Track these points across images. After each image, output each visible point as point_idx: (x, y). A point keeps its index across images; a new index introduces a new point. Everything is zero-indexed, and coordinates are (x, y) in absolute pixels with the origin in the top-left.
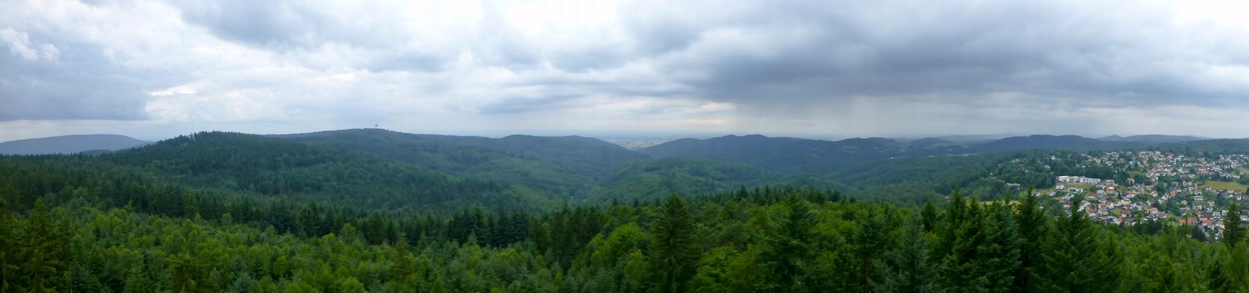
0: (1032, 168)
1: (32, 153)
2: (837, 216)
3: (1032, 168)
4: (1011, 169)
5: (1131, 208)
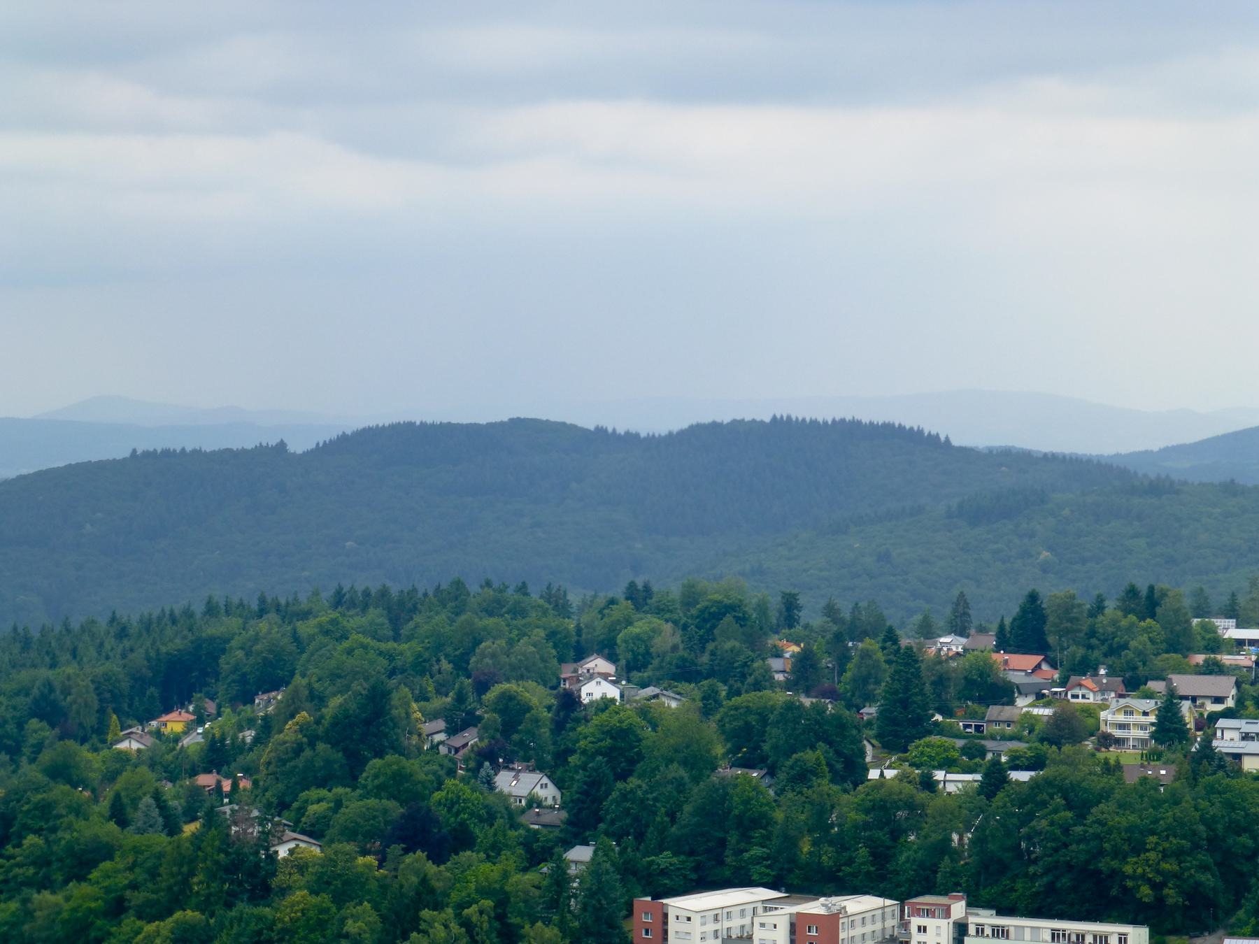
0: (356, 805)
3: (356, 805)
4: (100, 828)
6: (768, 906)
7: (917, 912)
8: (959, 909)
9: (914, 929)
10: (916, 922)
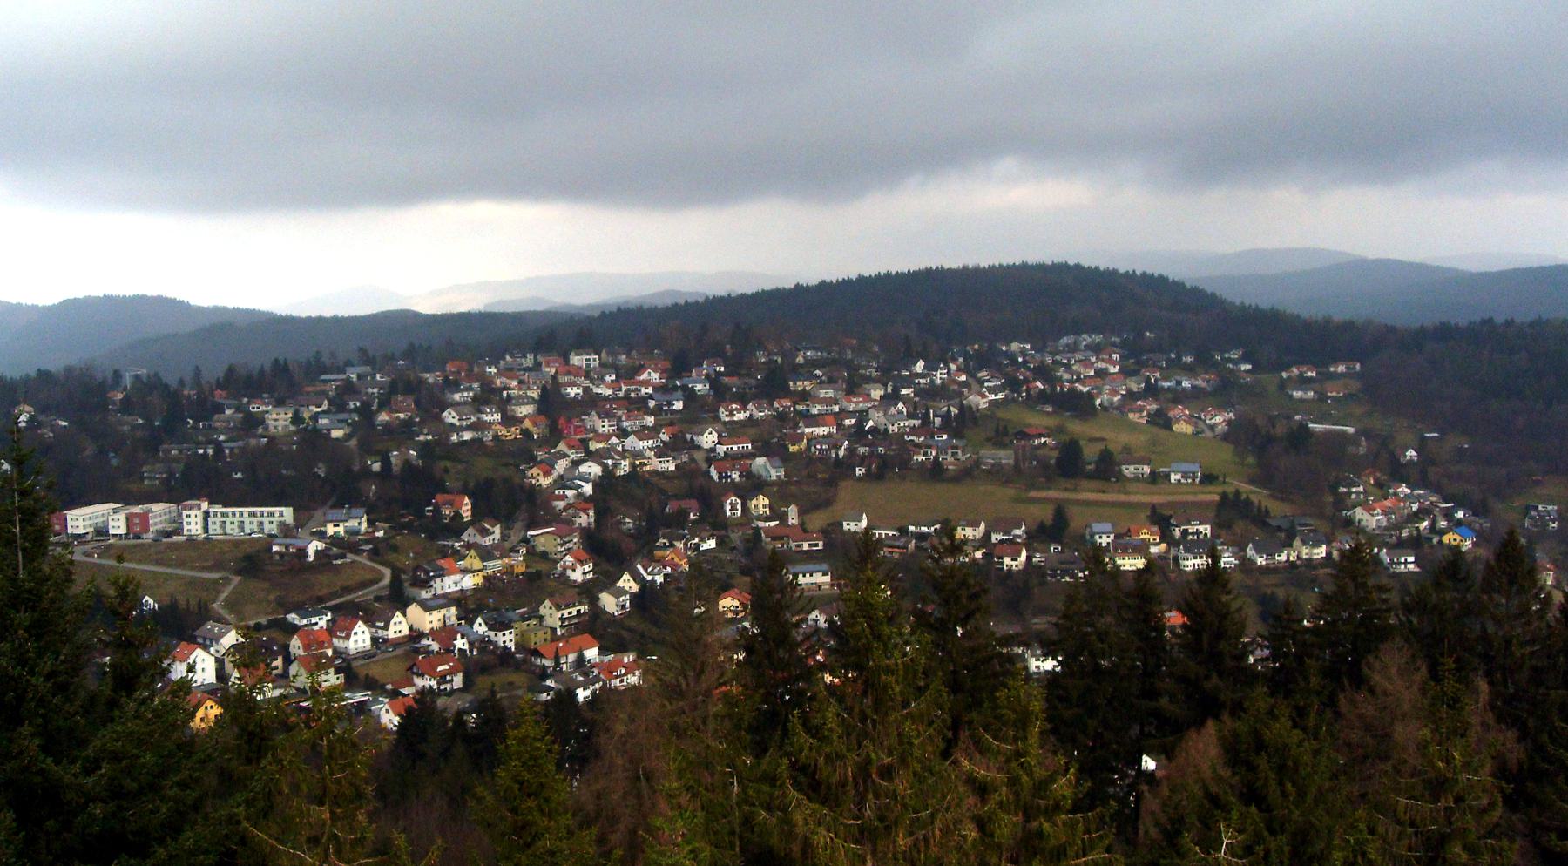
1: (1165, 273)
2: (1410, 755)
5: (460, 643)
6: (115, 511)
7: (185, 508)
8: (205, 505)
9: (184, 516)
10: (185, 513)
